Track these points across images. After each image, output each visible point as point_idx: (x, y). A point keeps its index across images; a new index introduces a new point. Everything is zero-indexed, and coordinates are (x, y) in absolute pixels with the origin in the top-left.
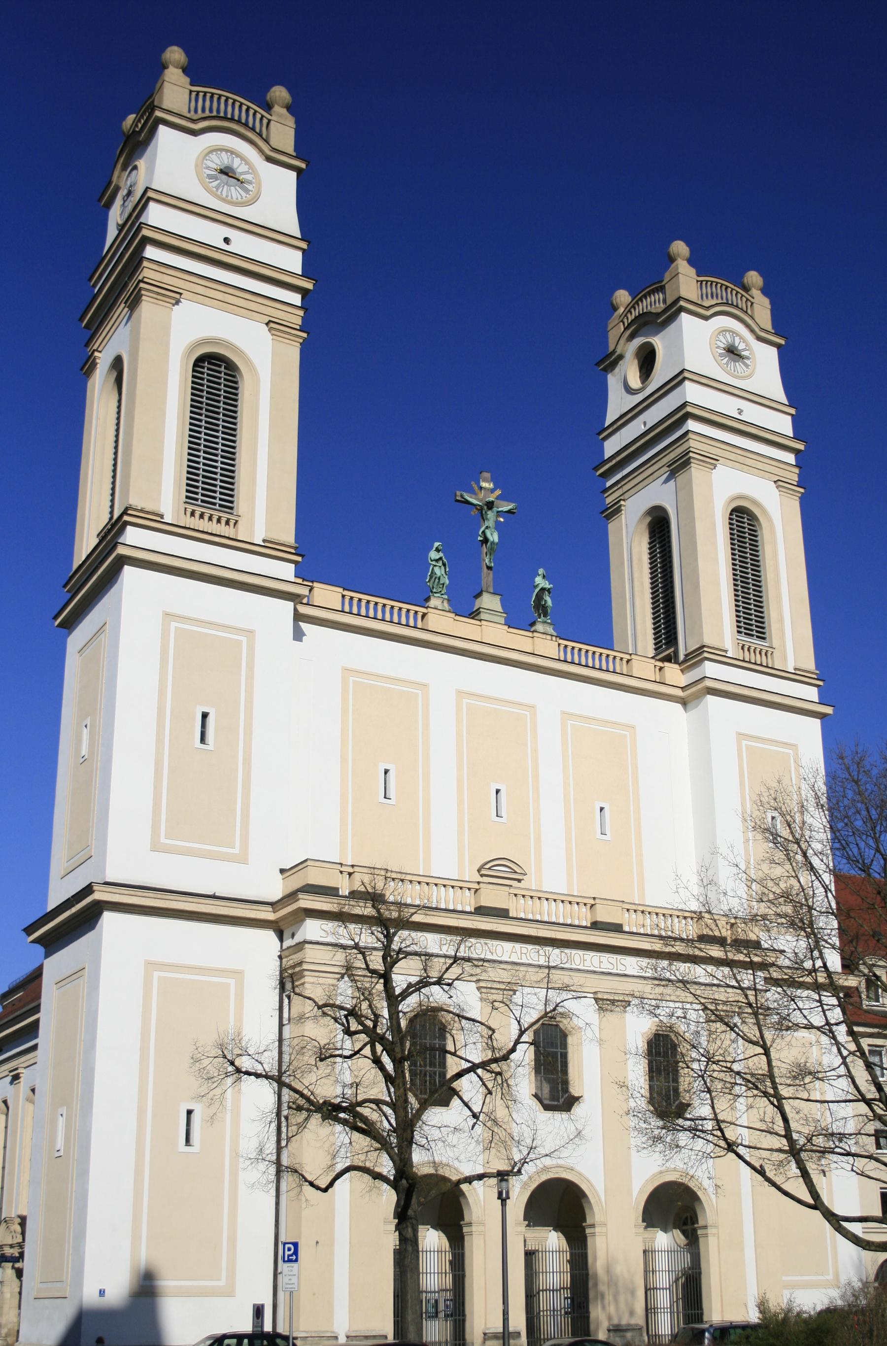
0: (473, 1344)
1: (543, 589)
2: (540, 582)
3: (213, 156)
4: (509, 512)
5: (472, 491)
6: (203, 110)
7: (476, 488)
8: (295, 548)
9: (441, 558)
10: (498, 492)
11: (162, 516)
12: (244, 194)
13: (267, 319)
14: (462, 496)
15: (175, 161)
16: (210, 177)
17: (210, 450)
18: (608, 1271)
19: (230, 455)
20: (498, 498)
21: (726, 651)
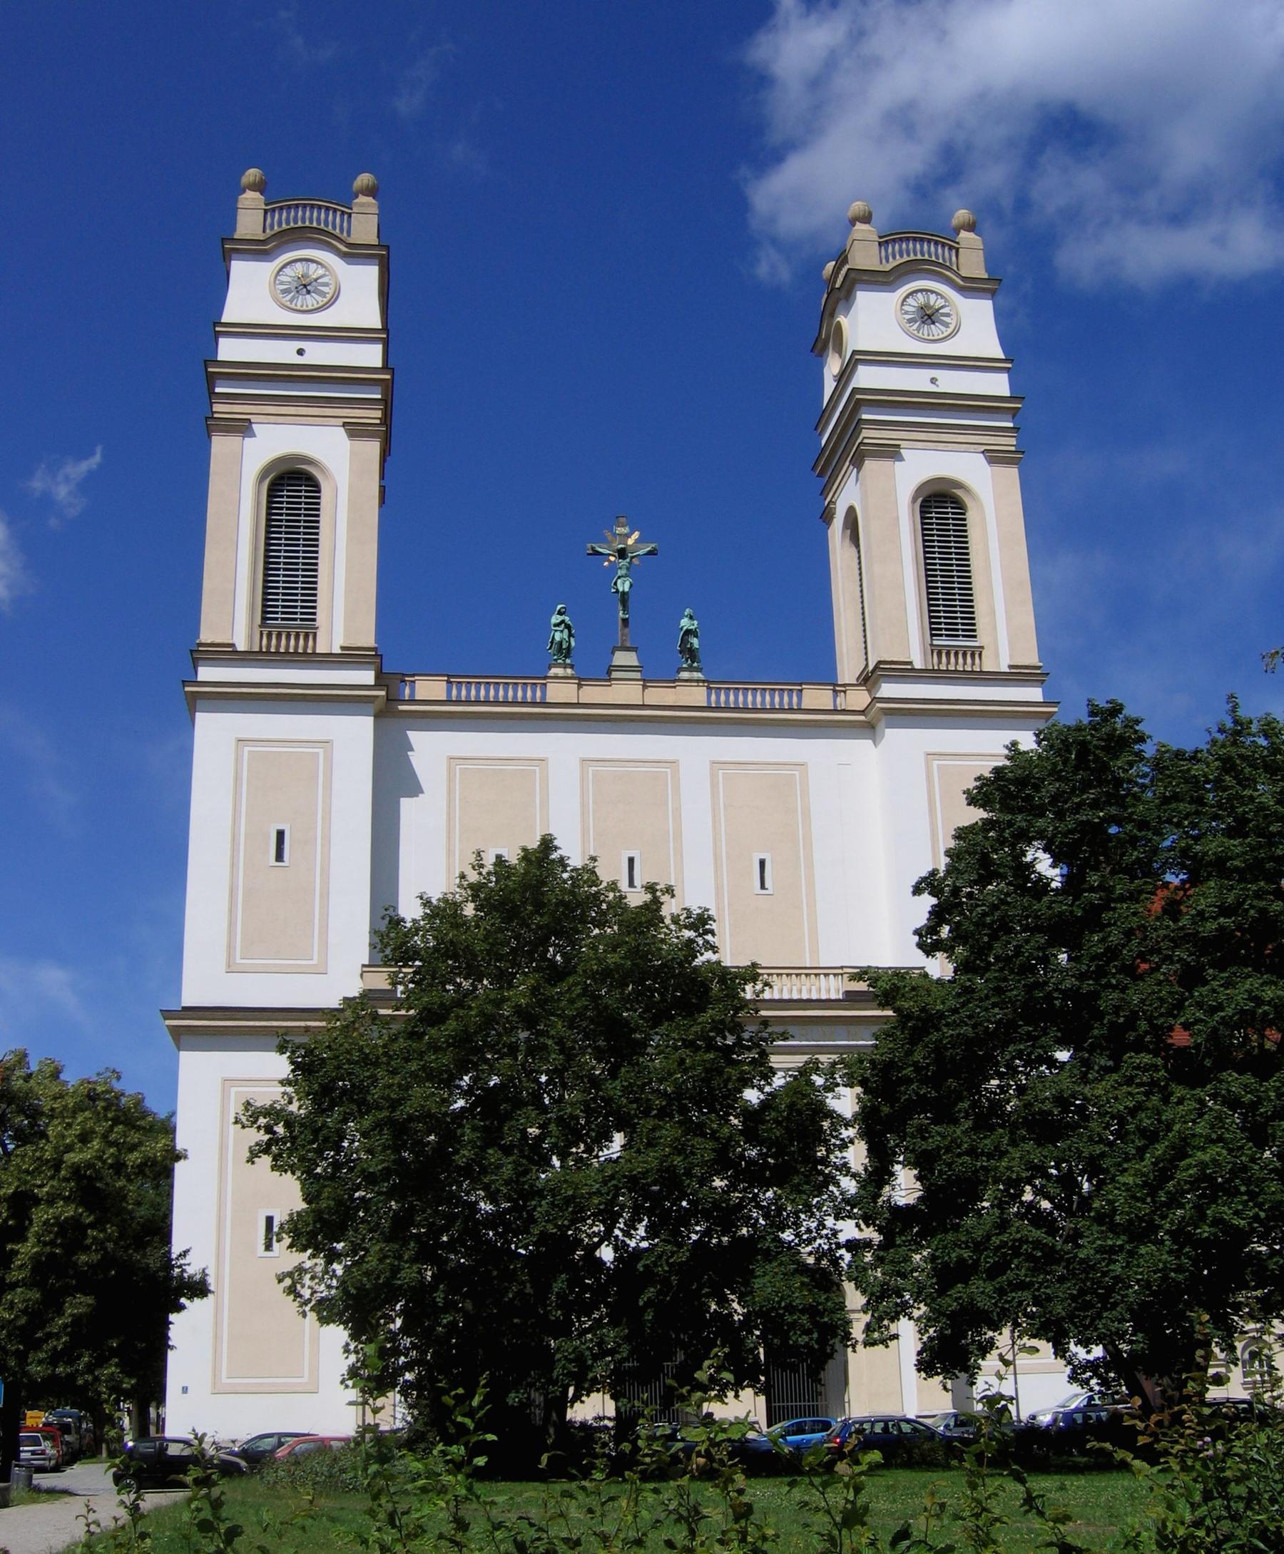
0: (4, 1504)
1: (688, 632)
2: (685, 623)
3: (910, 300)
4: (650, 553)
5: (604, 540)
6: (280, 224)
7: (610, 538)
8: (374, 649)
9: (563, 622)
10: (636, 535)
11: (233, 645)
12: (943, 328)
13: (341, 421)
14: (593, 548)
15: (251, 291)
16: (910, 321)
17: (945, 551)
18: (218, 1449)
19: (312, 567)
20: (637, 541)
21: (910, 663)
